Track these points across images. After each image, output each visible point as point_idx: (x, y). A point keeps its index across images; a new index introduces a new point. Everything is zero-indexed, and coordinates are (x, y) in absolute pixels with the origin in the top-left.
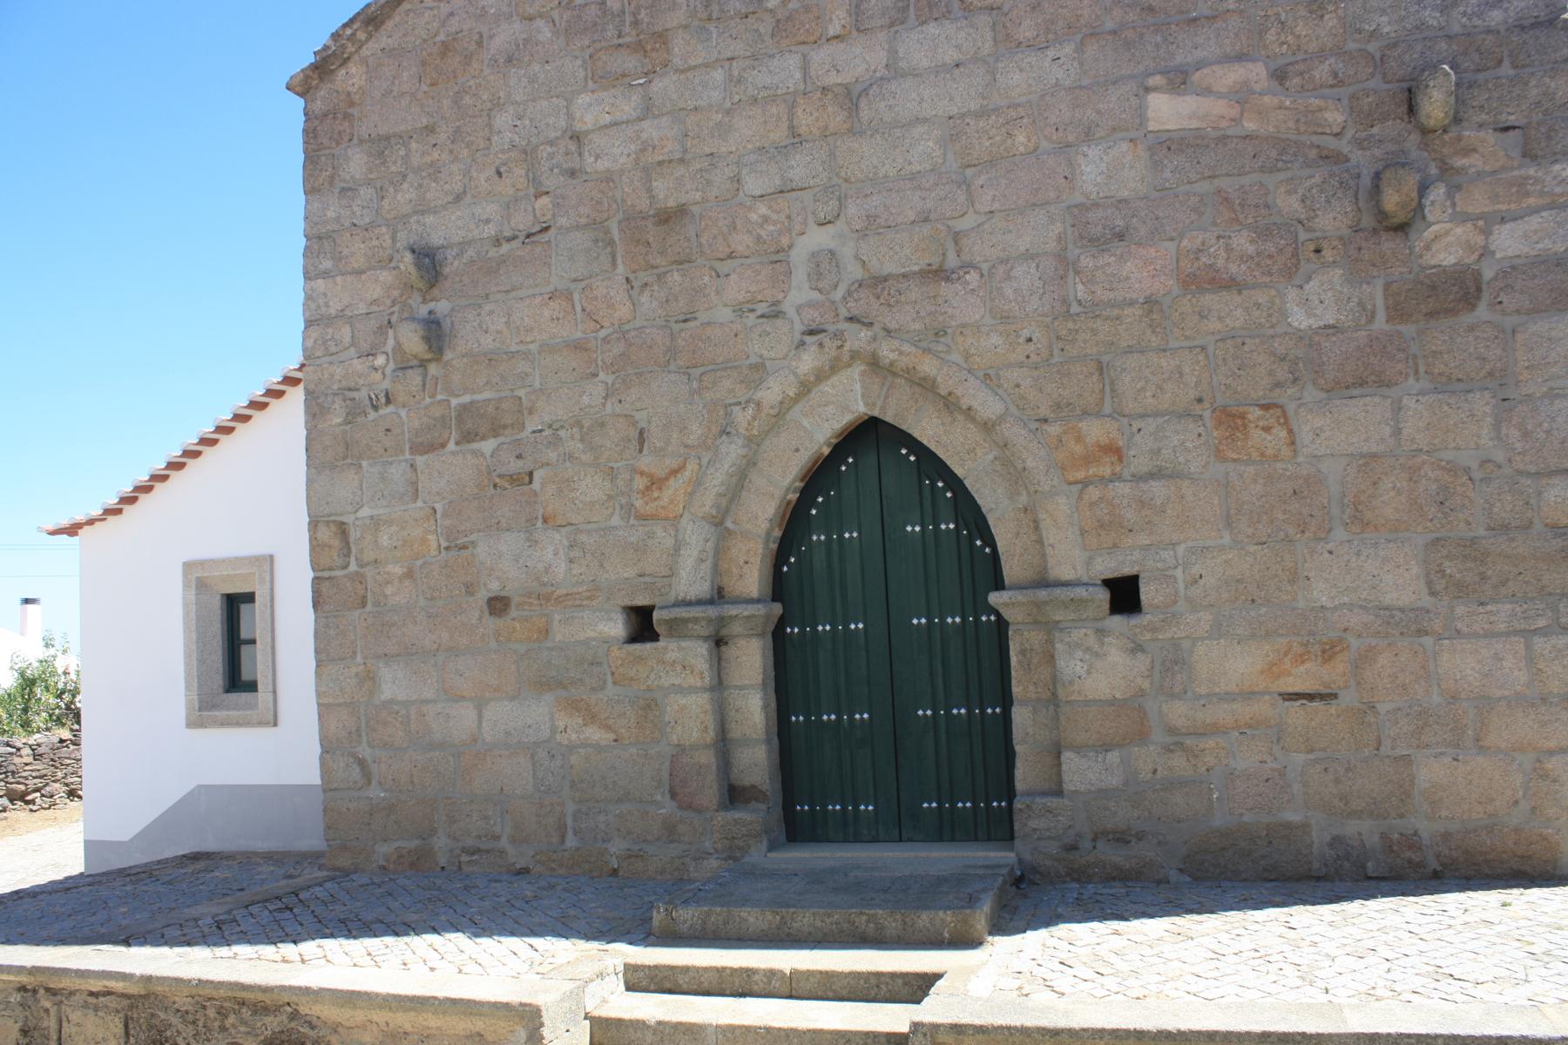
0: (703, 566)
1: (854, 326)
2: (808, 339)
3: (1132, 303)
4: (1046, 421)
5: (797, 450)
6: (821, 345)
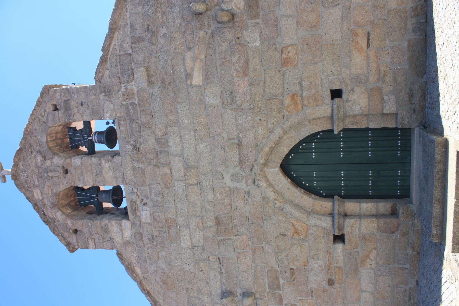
0: (322, 219)
3: (251, 90)
4: (284, 116)
5: (289, 189)
6: (258, 180)
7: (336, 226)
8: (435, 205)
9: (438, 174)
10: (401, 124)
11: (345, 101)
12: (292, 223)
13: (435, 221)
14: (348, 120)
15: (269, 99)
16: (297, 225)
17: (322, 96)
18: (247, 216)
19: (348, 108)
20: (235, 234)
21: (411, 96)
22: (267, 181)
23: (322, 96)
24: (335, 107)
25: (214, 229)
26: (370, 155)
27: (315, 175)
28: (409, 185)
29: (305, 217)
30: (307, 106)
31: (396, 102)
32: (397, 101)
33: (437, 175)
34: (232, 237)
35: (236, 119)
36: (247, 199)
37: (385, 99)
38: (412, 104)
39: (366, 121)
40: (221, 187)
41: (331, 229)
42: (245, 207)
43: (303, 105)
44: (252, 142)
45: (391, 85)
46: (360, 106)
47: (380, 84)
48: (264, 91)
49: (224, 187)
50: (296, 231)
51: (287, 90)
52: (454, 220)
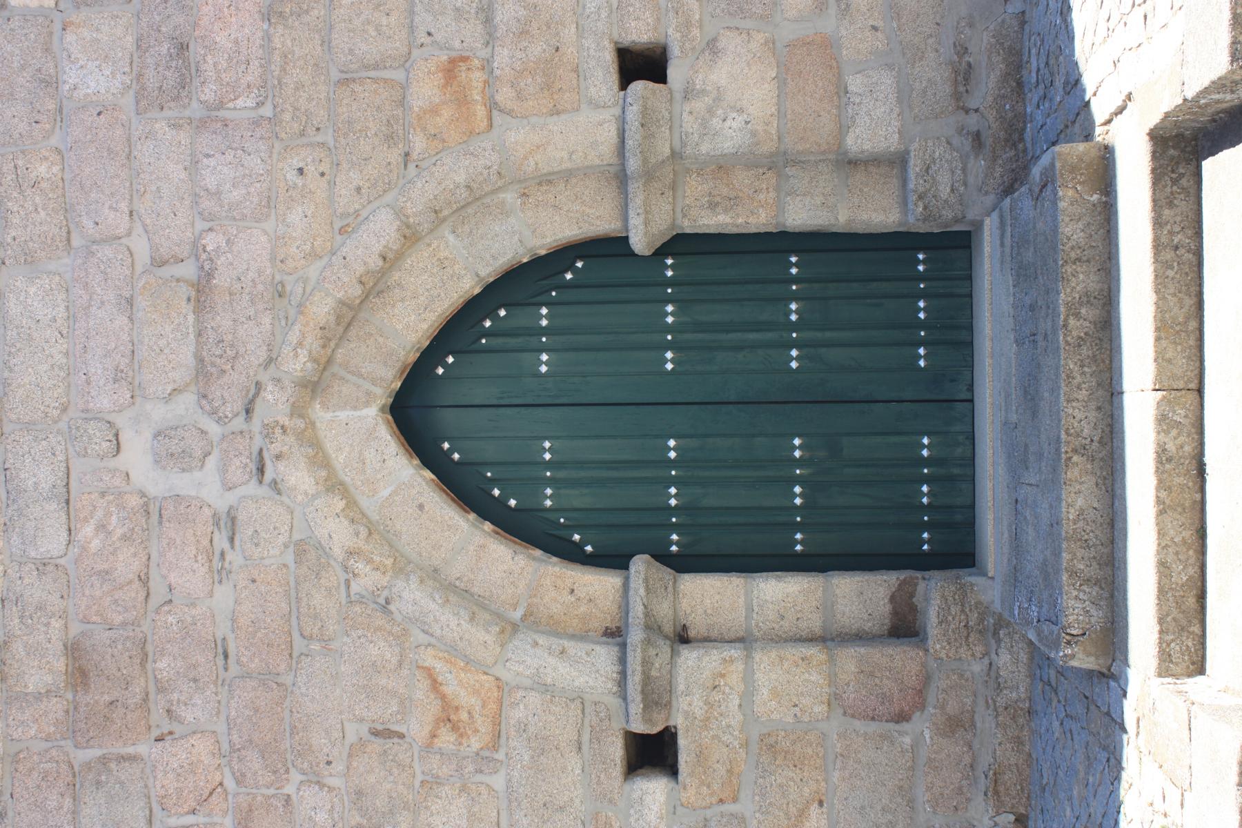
0: (572, 652)
3: (268, 37)
4: (407, 154)
5: (421, 507)
6: (278, 457)
7: (635, 681)
8: (1073, 473)
9: (1077, 316)
10: (920, 197)
11: (678, 96)
12: (429, 673)
13: (1076, 559)
14: (694, 189)
15: (344, 82)
16: (453, 685)
17: (576, 70)
18: (219, 636)
19: (690, 124)
20: (156, 733)
21: (963, 76)
22: (320, 460)
23: (576, 70)
24: (633, 113)
25: (56, 707)
26: (794, 365)
27: (547, 456)
28: (972, 506)
29: (490, 639)
30: (509, 113)
31: (900, 101)
32: (903, 96)
33: (1072, 322)
34: (142, 749)
35: (193, 166)
36: (222, 554)
37: (851, 88)
38: (967, 111)
39: (772, 194)
40: (103, 494)
41: (614, 702)
43: (492, 106)
44: (260, 272)
45: (875, 28)
46: (741, 119)
47: (828, 24)
48: (326, 43)
49: (120, 494)
50: (448, 717)
51: (428, 40)
52: (1159, 501)
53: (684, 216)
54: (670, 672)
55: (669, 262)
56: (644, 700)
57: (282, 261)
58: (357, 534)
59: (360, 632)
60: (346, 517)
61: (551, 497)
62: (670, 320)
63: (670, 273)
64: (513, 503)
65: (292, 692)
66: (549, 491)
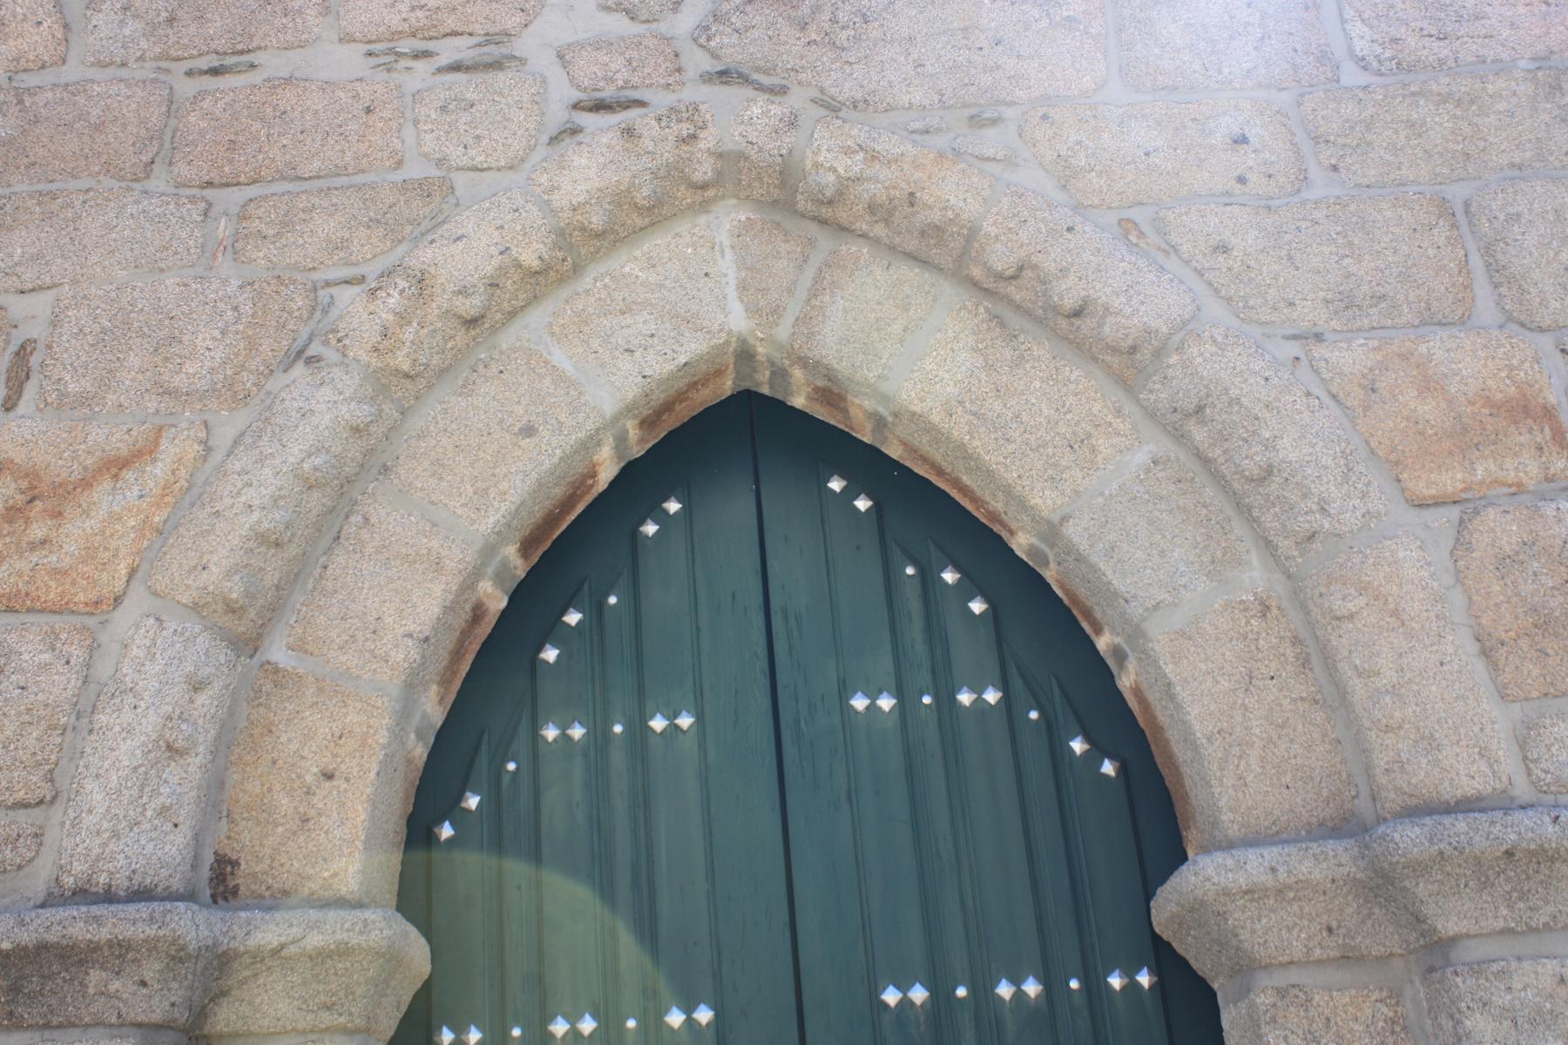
0: (173, 772)
1: (732, 94)
2: (588, 120)
3: (1502, 68)
4: (1319, 337)
5: (529, 431)
6: (629, 132)
27: (658, 724)
36: (426, 54)
41: (39, 880)
42: (347, 39)
53: (1282, 993)
54: (98, 1024)
55: (1144, 979)
56: (21, 952)
57: (1045, 117)
58: (463, 292)
59: (247, 309)
60: (502, 270)
61: (564, 737)
62: (1005, 990)
63: (1116, 982)
64: (550, 655)
65: (129, 189)
66: (577, 732)
